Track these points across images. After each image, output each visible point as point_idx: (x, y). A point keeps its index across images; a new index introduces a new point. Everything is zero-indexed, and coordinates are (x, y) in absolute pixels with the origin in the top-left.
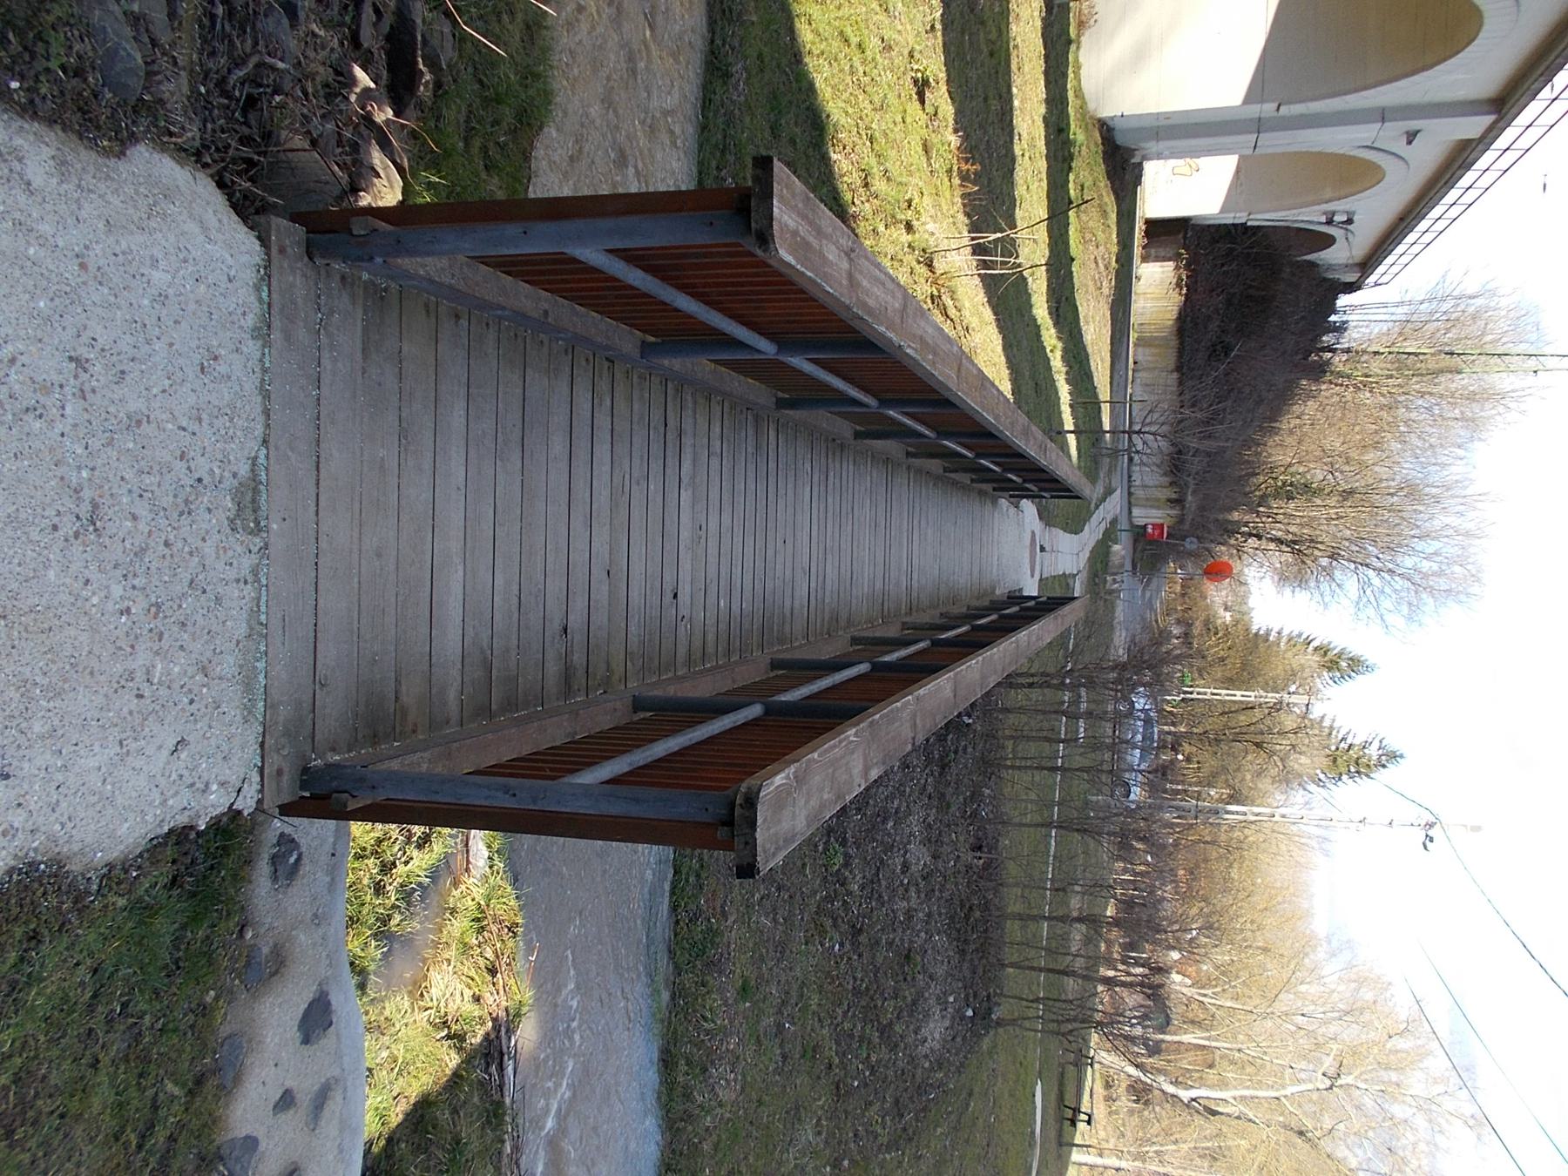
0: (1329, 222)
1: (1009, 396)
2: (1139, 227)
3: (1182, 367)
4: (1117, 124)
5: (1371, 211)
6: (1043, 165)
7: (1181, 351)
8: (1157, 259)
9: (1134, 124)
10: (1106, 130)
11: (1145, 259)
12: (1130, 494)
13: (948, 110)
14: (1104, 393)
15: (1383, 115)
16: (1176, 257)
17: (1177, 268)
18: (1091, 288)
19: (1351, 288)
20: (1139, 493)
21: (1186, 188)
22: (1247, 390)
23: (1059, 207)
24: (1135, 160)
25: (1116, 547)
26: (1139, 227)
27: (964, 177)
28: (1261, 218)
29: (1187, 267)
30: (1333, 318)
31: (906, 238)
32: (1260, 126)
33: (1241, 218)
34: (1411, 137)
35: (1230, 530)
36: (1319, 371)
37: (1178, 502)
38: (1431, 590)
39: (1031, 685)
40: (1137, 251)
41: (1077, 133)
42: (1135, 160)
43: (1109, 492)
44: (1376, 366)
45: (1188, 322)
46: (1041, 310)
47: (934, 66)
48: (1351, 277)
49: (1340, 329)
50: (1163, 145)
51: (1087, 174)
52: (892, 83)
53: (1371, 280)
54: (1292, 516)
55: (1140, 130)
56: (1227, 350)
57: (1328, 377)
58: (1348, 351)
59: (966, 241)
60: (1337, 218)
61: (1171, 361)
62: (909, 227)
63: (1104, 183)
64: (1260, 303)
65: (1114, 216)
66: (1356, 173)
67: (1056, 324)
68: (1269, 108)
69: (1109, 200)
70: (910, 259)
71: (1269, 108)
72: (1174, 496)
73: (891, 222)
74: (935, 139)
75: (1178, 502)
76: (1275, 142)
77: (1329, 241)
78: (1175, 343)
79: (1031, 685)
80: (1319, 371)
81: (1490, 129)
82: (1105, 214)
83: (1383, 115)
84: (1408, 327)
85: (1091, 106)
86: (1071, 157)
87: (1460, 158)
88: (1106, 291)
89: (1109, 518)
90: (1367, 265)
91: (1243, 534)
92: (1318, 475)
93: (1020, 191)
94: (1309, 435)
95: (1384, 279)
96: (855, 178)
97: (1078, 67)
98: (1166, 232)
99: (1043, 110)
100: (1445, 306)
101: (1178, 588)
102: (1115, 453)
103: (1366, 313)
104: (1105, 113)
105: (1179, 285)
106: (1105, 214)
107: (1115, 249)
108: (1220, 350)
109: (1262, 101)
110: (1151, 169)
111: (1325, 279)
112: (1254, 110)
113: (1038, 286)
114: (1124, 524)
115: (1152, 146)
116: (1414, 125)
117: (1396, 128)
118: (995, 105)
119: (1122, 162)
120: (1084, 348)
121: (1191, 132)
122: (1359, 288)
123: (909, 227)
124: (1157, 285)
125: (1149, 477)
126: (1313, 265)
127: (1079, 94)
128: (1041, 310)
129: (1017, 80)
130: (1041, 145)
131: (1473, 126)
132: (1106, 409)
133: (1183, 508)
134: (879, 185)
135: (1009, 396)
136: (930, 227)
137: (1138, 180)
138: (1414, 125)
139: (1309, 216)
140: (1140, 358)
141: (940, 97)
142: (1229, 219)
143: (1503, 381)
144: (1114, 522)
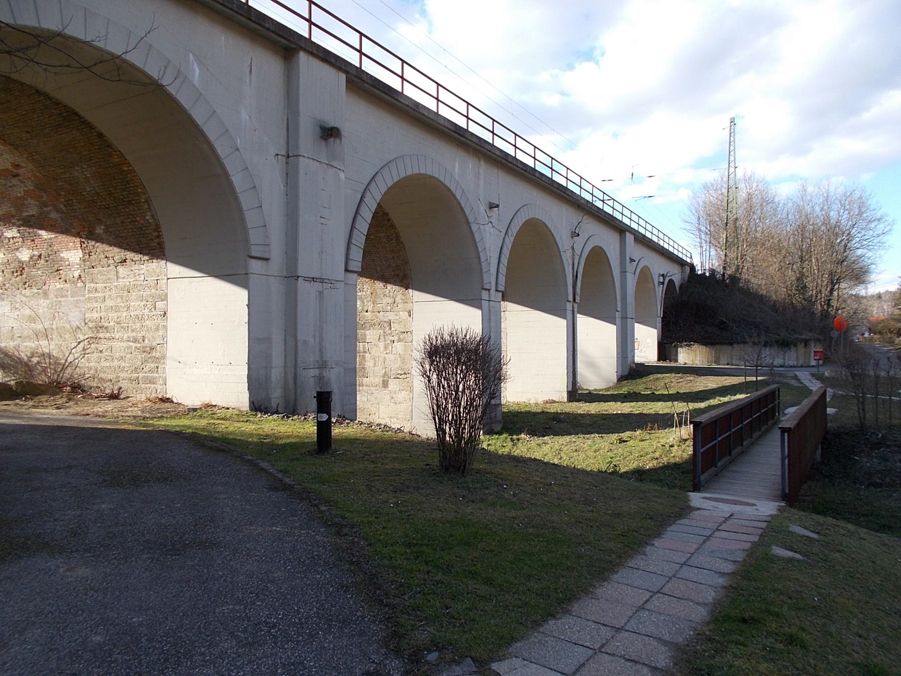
0: (663, 283)
1: (677, 288)
2: (661, 364)
3: (731, 343)
4: (620, 374)
5: (659, 267)
6: (640, 403)
7: (722, 344)
8: (677, 355)
9: (620, 369)
10: (621, 379)
11: (676, 361)
12: (802, 366)
13: (628, 433)
14: (742, 379)
15: (623, 272)
16: (676, 347)
17: (681, 347)
18: (690, 384)
19: (692, 267)
20: (801, 362)
21: (646, 344)
22: (744, 312)
23: (654, 398)
24: (634, 366)
25: (826, 374)
26: (661, 364)
27: (652, 429)
28: (660, 312)
29: (681, 342)
30: (707, 274)
31: (676, 447)
32: (624, 318)
33: (659, 320)
34: (632, 260)
35: (825, 315)
36: (734, 279)
37: (806, 343)
38: (860, 214)
39: (864, 410)
40: (673, 364)
41: (624, 390)
42: (634, 366)
43: (796, 378)
44: (732, 255)
45: (706, 341)
46: (702, 405)
47: (614, 437)
48: (688, 269)
49: (713, 271)
50: (629, 356)
51: (640, 386)
52: (621, 449)
53: (689, 260)
54: (816, 284)
55: (622, 365)
56: (722, 322)
57: (738, 275)
58: (724, 268)
59: (678, 429)
60: (661, 280)
61: (727, 349)
62: (672, 446)
63: (644, 380)
64: (698, 307)
65: (659, 375)
66: (644, 276)
67: (708, 399)
68: (618, 315)
69: (652, 377)
70: (683, 447)
71: (618, 315)
72: (803, 344)
73: (670, 451)
74: (639, 438)
75: (806, 343)
76: (631, 312)
77: (671, 282)
78: (718, 347)
79: (864, 410)
80: (734, 279)
81: (631, 233)
82: (658, 379)
83: (623, 272)
84: (713, 239)
85: (612, 385)
86: (634, 393)
87: (642, 240)
88: (692, 378)
89: (810, 377)
90: (681, 263)
91: (828, 308)
92: (791, 276)
93: (652, 412)
94: (769, 278)
95: (689, 255)
96: (655, 462)
97: (596, 390)
98: (665, 350)
99: (619, 403)
100: (703, 228)
101: (877, 336)
102: (772, 374)
103: (703, 257)
104: (615, 379)
105: (689, 346)
106: (658, 379)
107: (673, 375)
108: (723, 326)
109: (615, 317)
110: (637, 360)
111: (688, 281)
112: (618, 320)
113: (692, 406)
114: (814, 370)
115: (629, 360)
116: (628, 260)
117: (630, 267)
118: (622, 419)
119: (633, 372)
120: (719, 388)
121: (625, 343)
122: (693, 265)
123: (672, 446)
124: (686, 356)
125: (791, 357)
126: (680, 288)
127: (608, 389)
128: (702, 405)
129: (611, 412)
130: (633, 404)
131: (629, 238)
132: (749, 379)
133: (810, 340)
134: (657, 455)
135: (677, 288)
136: (671, 439)
137: (642, 365)
138: (628, 260)
139: (660, 291)
140: (726, 362)
141: (626, 435)
142: (659, 325)
143: (742, 195)
144: (813, 375)
